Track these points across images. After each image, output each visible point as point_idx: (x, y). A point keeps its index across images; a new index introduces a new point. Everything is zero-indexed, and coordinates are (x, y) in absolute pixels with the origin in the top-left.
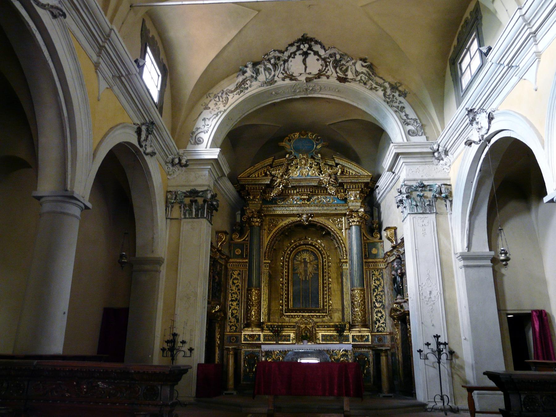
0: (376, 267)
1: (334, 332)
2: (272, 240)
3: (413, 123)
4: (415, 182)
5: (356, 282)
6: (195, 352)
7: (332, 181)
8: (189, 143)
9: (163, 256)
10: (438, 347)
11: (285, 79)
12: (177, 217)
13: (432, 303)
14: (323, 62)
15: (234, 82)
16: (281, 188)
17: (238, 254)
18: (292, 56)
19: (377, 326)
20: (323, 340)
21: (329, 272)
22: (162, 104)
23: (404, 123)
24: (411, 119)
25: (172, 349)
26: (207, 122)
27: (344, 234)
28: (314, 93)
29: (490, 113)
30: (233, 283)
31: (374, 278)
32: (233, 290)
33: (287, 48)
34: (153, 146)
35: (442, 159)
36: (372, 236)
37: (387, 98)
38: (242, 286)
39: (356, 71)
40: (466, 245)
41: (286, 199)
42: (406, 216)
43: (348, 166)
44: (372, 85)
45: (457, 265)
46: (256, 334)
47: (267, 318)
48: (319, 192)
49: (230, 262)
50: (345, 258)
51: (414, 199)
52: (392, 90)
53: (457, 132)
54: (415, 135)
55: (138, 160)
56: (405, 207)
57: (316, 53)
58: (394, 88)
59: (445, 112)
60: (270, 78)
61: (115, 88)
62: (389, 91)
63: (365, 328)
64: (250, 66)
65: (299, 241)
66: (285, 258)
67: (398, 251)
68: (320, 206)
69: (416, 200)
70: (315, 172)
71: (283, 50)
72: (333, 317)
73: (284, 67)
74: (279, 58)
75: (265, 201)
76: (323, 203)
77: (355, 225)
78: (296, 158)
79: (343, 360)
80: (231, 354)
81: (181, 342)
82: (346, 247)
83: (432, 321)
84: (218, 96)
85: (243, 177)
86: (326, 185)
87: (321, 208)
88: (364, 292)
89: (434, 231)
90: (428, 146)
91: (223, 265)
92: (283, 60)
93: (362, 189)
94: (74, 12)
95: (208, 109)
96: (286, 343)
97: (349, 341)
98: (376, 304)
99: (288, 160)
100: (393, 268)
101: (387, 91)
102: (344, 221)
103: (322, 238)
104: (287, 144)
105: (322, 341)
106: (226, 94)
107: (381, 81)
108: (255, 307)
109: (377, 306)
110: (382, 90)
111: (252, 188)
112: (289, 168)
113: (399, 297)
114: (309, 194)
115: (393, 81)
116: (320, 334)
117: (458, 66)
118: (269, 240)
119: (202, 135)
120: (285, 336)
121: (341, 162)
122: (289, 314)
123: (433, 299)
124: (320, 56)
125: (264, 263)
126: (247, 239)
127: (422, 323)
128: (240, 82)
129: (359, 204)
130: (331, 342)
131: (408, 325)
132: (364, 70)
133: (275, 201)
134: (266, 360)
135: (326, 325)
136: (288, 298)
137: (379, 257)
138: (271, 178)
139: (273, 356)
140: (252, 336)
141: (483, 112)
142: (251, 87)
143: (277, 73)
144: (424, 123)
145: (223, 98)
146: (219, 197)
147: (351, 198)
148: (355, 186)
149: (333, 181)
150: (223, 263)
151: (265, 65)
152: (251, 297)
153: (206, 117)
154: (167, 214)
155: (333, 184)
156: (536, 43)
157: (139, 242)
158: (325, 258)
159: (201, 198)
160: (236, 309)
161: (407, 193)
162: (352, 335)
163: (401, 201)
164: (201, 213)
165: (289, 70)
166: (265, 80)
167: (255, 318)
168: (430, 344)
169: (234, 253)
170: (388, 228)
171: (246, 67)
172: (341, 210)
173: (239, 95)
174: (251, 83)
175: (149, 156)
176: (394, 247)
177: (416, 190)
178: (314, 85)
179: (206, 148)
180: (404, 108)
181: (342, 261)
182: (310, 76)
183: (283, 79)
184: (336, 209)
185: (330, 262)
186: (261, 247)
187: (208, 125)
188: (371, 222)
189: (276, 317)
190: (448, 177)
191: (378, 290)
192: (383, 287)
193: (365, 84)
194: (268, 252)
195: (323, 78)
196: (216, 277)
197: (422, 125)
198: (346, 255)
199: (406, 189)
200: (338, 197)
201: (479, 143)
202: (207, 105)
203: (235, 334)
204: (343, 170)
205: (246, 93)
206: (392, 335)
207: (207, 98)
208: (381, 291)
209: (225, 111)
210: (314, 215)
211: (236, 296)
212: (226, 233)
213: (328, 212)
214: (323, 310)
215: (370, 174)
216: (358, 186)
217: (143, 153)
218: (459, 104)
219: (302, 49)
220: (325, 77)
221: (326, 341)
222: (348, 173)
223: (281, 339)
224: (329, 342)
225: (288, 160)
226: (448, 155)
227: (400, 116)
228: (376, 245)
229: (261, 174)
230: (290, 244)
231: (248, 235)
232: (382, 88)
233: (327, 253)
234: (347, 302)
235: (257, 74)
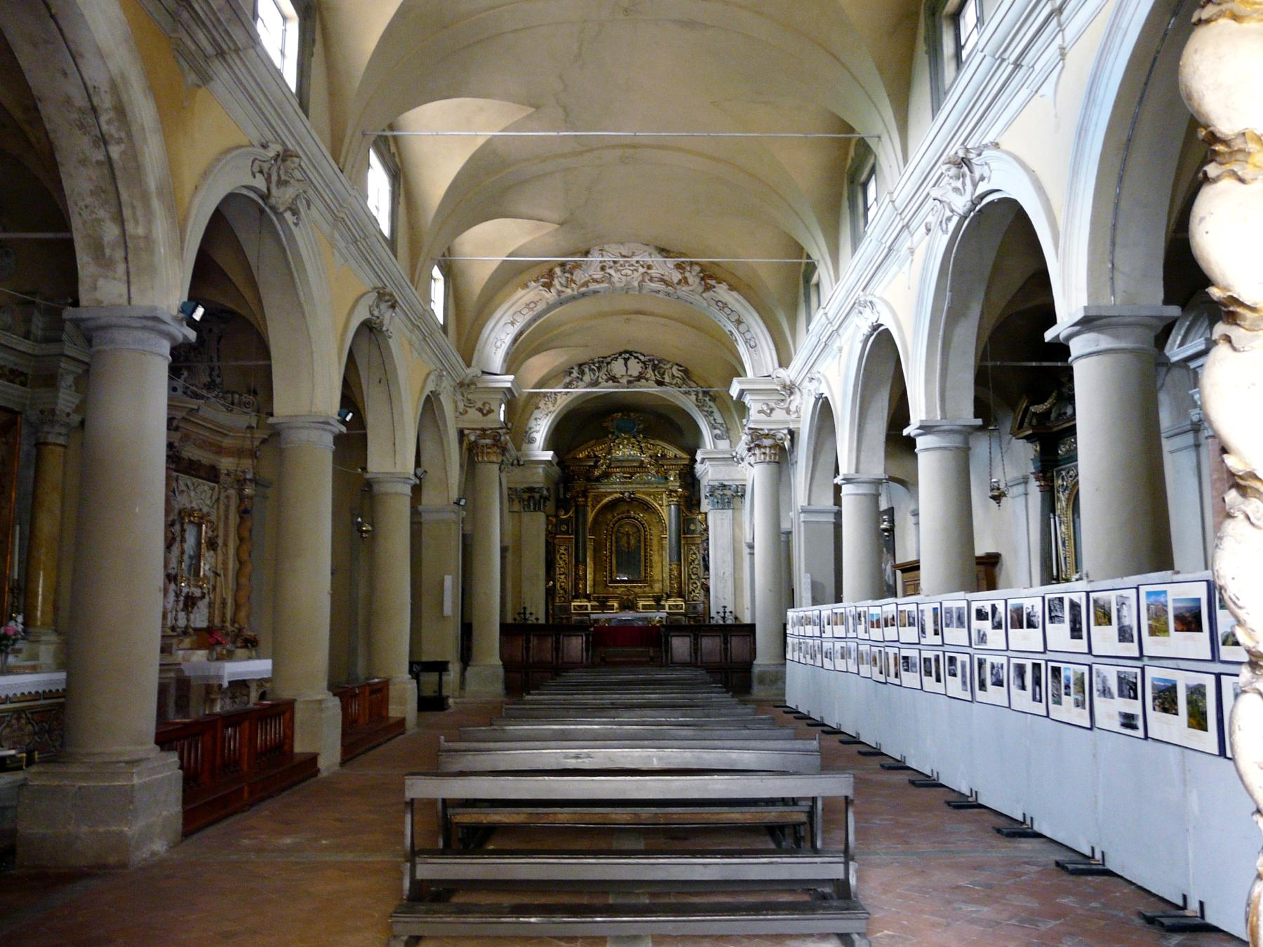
26: (539, 422)
39: (673, 375)
62: (700, 395)
64: (576, 368)
75: (589, 479)
94: (246, 103)
105: (1059, 668)
119: (535, 435)
124: (640, 360)
129: (678, 484)
136: (611, 570)
140: (580, 607)
156: (1061, 28)
180: (712, 412)
182: (630, 379)
214: (645, 581)
234: (666, 575)
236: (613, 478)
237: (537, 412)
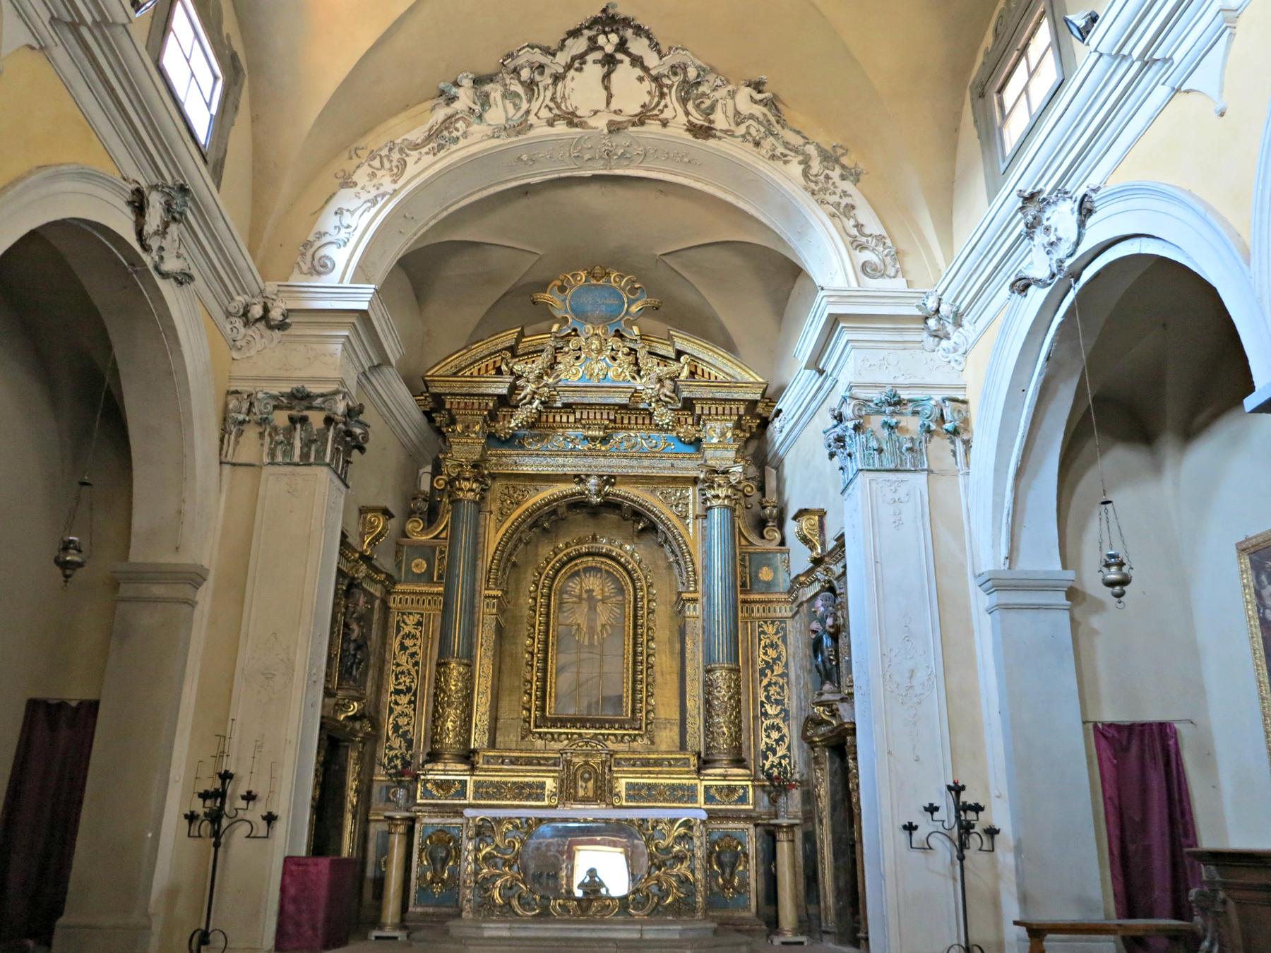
0: (769, 615)
2: (509, 539)
5: (720, 651)
6: (281, 827)
7: (666, 396)
8: (296, 271)
9: (205, 563)
10: (958, 817)
12: (252, 461)
13: (915, 700)
17: (419, 572)
18: (577, 65)
22: (221, 155)
25: (215, 817)
26: (347, 219)
27: (691, 530)
29: (1085, 195)
30: (403, 647)
31: (763, 643)
33: (564, 40)
34: (186, 255)
35: (947, 337)
36: (762, 537)
37: (812, 181)
38: (425, 655)
39: (737, 113)
40: (1004, 552)
41: (548, 435)
42: (851, 477)
43: (707, 359)
45: (980, 602)
46: (454, 781)
47: (486, 739)
48: (633, 421)
52: (825, 163)
53: (991, 260)
55: (141, 292)
56: (850, 455)
57: (637, 61)
58: (829, 158)
59: (955, 225)
60: (515, 118)
61: (59, 53)
62: (816, 166)
63: (738, 767)
64: (467, 83)
65: (577, 544)
66: (540, 587)
67: (827, 570)
71: (554, 46)
72: (657, 740)
73: (554, 93)
74: (541, 67)
77: (720, 506)
79: (680, 851)
81: (243, 798)
82: (696, 561)
83: (914, 748)
84: (381, 156)
85: (441, 376)
87: (634, 463)
88: (738, 677)
89: (923, 516)
90: (914, 301)
91: (377, 598)
93: (740, 417)
97: (696, 802)
98: (768, 707)
99: (556, 337)
100: (812, 615)
101: (811, 163)
102: (691, 498)
103: (636, 540)
104: (555, 298)
105: (627, 801)
106: (401, 151)
107: (796, 140)
108: (456, 709)
110: (800, 163)
111: (462, 405)
112: (559, 359)
113: (827, 687)
114: (606, 427)
115: (827, 142)
116: (623, 781)
117: (995, 98)
118: (501, 540)
119: (330, 251)
122: (546, 730)
123: (918, 690)
124: (646, 69)
125: (486, 597)
126: (443, 535)
127: (889, 753)
128: (439, 122)
129: (732, 454)
130: (651, 804)
131: (850, 761)
132: (758, 110)
137: (777, 589)
138: (511, 380)
139: (498, 839)
140: (443, 786)
141: (1064, 200)
143: (535, 105)
144: (902, 246)
145: (391, 161)
146: (367, 417)
147: (712, 438)
149: (668, 393)
150: (378, 594)
151: (506, 85)
153: (345, 206)
154: (224, 452)
155: (666, 402)
157: (139, 520)
158: (642, 590)
160: (406, 715)
163: (840, 439)
164: (317, 451)
166: (503, 121)
167: (455, 737)
168: (937, 809)
169: (409, 570)
170: (801, 513)
171: (456, 84)
172: (686, 469)
173: (434, 154)
174: (467, 127)
175: (172, 280)
176: (817, 562)
179: (341, 281)
180: (853, 207)
181: (685, 596)
183: (551, 123)
184: (672, 465)
185: (654, 601)
186: (480, 556)
187: (348, 227)
188: (761, 503)
189: (511, 736)
190: (961, 382)
191: (773, 672)
192: (786, 665)
193: (757, 144)
194: (498, 570)
196: (355, 626)
198: (696, 584)
199: (855, 406)
200: (678, 437)
201: (1049, 282)
202: (350, 176)
206: (805, 788)
207: (351, 158)
208: (782, 675)
211: (408, 681)
212: (386, 513)
213: (654, 472)
217: (151, 267)
218: (992, 192)
219: (602, 48)
221: (638, 801)
223: (521, 794)
224: (646, 804)
225: (556, 337)
226: (960, 326)
229: (487, 371)
230: (553, 551)
231: (446, 526)
232: (801, 158)
233: (646, 578)
235: (482, 105)
236: (558, 441)
237: (345, 193)
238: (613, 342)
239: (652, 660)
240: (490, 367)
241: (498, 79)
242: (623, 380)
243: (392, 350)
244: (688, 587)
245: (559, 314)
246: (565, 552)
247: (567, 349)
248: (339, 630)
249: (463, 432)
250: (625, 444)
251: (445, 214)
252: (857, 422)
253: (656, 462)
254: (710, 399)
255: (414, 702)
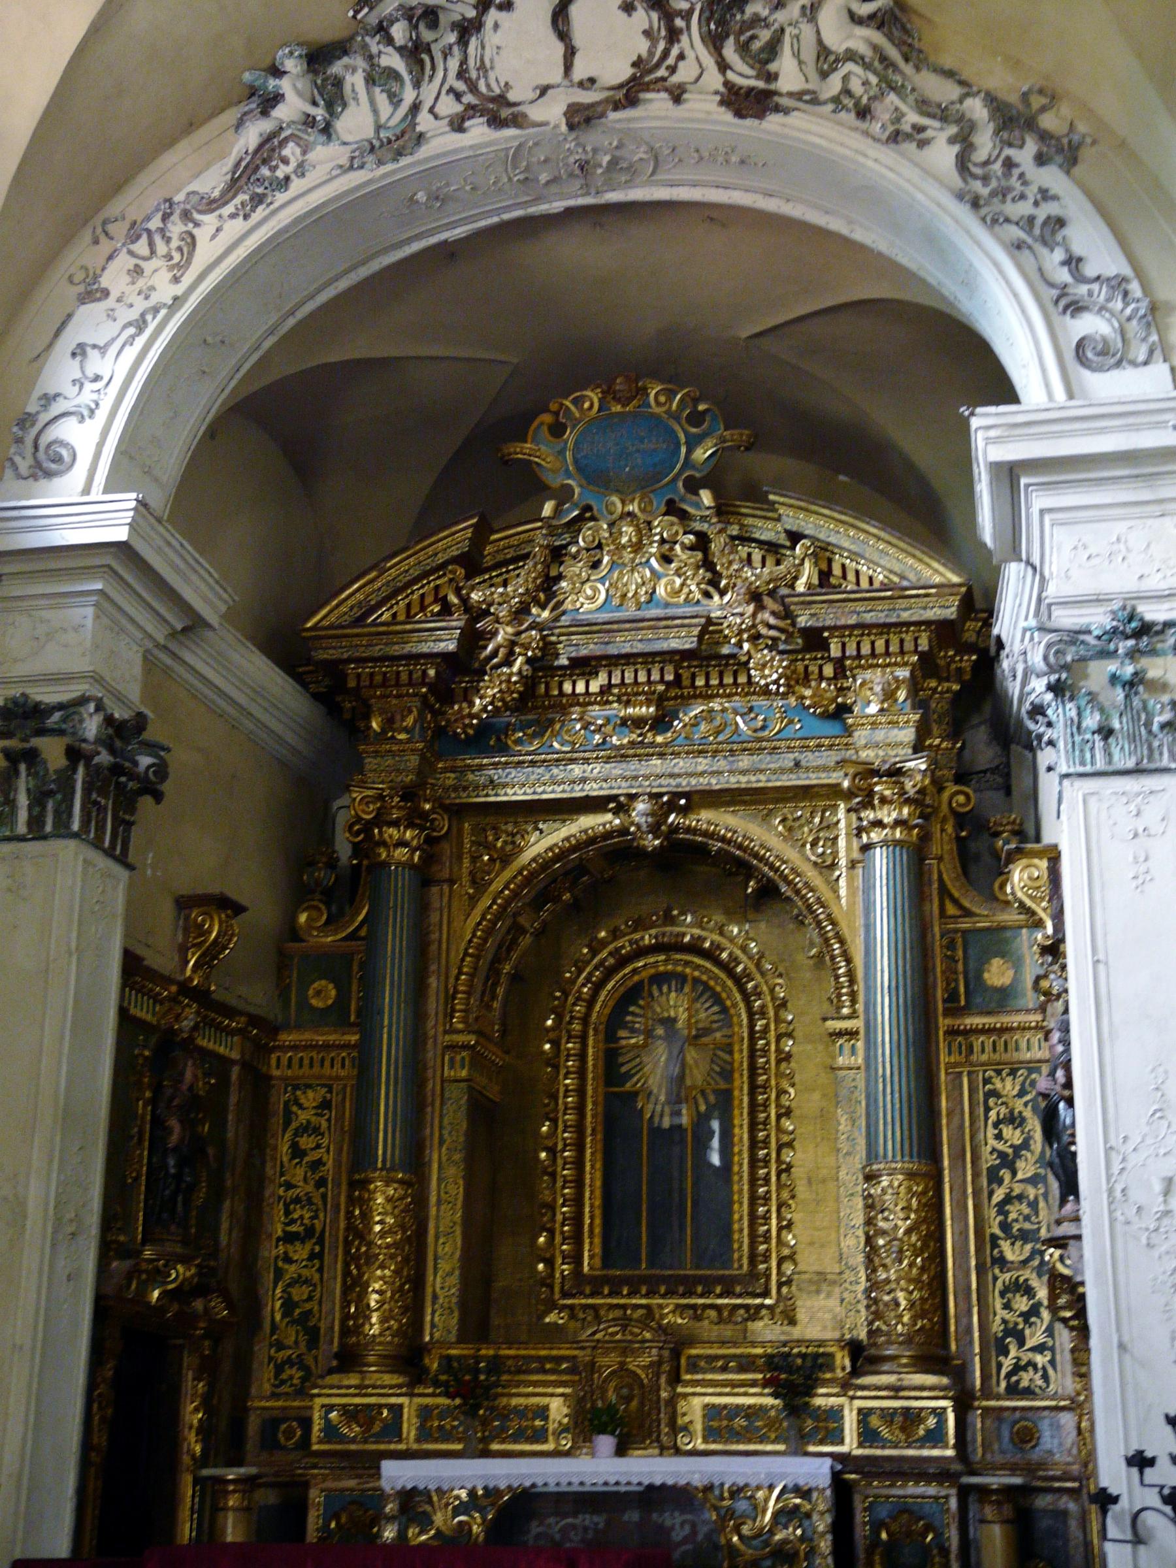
0: (1006, 1057)
1: (761, 1395)
3: (1108, 300)
4: (1101, 610)
7: (770, 627)
8: (9, 473)
11: (463, 120)
14: (655, 16)
15: (223, 156)
16: (520, 672)
19: (1008, 1363)
20: (710, 1434)
21: (785, 1084)
23: (1057, 302)
24: (1098, 278)
26: (96, 364)
27: (843, 892)
28: (629, 184)
30: (297, 1152)
31: (993, 1115)
32: (295, 1187)
37: (975, 177)
39: (823, 51)
41: (551, 722)
44: (898, 117)
48: (714, 682)
49: (283, 1048)
50: (845, 1011)
51: (1092, 697)
52: (1005, 135)
54: (1113, 361)
60: (392, 123)
62: (985, 143)
63: (926, 1372)
64: (292, 65)
65: (635, 931)
68: (716, 751)
69: (1107, 704)
70: (683, 585)
73: (464, 61)
76: (735, 738)
77: (885, 843)
78: (587, 514)
80: (235, 1509)
84: (149, 231)
86: (739, 645)
87: (721, 764)
91: (233, 1062)
92: (455, 26)
95: (99, 300)
96: (527, 1447)
98: (1005, 1246)
105: (705, 1440)
106: (186, 216)
107: (943, 91)
109: (1010, 1256)
110: (952, 141)
116: (697, 1403)
119: (71, 432)
120: (522, 1412)
121: (808, 524)
127: (1122, 1347)
129: (907, 735)
132: (861, 39)
133: (499, 739)
134: (402, 1535)
135: (734, 1357)
142: (303, 175)
143: (429, 92)
145: (168, 240)
148: (887, 642)
149: (772, 621)
152: (366, 1216)
155: (774, 639)
159: (56, 739)
160: (307, 1282)
161: (1051, 669)
162: (860, 1410)
164: (57, 813)
165: (486, 78)
166: (370, 133)
168: (1151, 1462)
169: (304, 1003)
171: (277, 72)
174: (304, 153)
177: (1106, 654)
178: (615, 143)
179: (87, 491)
180: (1060, 222)
183: (458, 124)
184: (797, 764)
187: (97, 378)
191: (1014, 1173)
193: (863, 113)
195: (651, 101)
196: (174, 1123)
197: (1153, 308)
198: (854, 1001)
199: (1049, 646)
202: (96, 278)
203: (296, 1404)
204: (824, 567)
205: (276, 205)
207: (96, 242)
209: (178, 301)
210: (696, 798)
212: (227, 905)
213: (760, 781)
215: (955, 579)
216: (902, 641)
220: (664, 95)
221: (726, 1442)
222: (851, 576)
227: (1040, 269)
228: (1006, 941)
230: (589, 946)
232: (953, 130)
233: (772, 991)
235: (330, 106)
238: (662, 526)
239: (788, 1156)
240: (429, 599)
241: (355, 46)
242: (687, 600)
243: (206, 600)
244: (839, 1008)
245: (555, 481)
246: (611, 947)
247: (574, 549)
248: (141, 1133)
249: (384, 731)
250: (703, 727)
251: (291, 322)
252: (1054, 678)
253: (765, 760)
254: (853, 627)
255: (320, 1256)
